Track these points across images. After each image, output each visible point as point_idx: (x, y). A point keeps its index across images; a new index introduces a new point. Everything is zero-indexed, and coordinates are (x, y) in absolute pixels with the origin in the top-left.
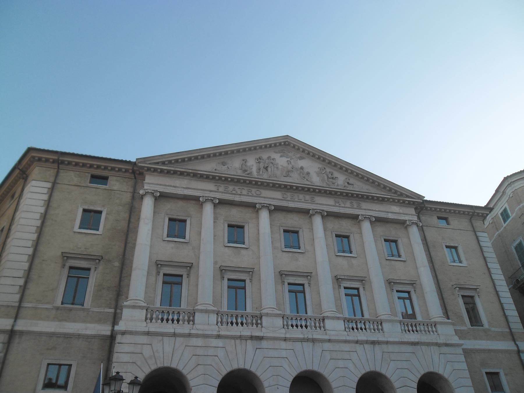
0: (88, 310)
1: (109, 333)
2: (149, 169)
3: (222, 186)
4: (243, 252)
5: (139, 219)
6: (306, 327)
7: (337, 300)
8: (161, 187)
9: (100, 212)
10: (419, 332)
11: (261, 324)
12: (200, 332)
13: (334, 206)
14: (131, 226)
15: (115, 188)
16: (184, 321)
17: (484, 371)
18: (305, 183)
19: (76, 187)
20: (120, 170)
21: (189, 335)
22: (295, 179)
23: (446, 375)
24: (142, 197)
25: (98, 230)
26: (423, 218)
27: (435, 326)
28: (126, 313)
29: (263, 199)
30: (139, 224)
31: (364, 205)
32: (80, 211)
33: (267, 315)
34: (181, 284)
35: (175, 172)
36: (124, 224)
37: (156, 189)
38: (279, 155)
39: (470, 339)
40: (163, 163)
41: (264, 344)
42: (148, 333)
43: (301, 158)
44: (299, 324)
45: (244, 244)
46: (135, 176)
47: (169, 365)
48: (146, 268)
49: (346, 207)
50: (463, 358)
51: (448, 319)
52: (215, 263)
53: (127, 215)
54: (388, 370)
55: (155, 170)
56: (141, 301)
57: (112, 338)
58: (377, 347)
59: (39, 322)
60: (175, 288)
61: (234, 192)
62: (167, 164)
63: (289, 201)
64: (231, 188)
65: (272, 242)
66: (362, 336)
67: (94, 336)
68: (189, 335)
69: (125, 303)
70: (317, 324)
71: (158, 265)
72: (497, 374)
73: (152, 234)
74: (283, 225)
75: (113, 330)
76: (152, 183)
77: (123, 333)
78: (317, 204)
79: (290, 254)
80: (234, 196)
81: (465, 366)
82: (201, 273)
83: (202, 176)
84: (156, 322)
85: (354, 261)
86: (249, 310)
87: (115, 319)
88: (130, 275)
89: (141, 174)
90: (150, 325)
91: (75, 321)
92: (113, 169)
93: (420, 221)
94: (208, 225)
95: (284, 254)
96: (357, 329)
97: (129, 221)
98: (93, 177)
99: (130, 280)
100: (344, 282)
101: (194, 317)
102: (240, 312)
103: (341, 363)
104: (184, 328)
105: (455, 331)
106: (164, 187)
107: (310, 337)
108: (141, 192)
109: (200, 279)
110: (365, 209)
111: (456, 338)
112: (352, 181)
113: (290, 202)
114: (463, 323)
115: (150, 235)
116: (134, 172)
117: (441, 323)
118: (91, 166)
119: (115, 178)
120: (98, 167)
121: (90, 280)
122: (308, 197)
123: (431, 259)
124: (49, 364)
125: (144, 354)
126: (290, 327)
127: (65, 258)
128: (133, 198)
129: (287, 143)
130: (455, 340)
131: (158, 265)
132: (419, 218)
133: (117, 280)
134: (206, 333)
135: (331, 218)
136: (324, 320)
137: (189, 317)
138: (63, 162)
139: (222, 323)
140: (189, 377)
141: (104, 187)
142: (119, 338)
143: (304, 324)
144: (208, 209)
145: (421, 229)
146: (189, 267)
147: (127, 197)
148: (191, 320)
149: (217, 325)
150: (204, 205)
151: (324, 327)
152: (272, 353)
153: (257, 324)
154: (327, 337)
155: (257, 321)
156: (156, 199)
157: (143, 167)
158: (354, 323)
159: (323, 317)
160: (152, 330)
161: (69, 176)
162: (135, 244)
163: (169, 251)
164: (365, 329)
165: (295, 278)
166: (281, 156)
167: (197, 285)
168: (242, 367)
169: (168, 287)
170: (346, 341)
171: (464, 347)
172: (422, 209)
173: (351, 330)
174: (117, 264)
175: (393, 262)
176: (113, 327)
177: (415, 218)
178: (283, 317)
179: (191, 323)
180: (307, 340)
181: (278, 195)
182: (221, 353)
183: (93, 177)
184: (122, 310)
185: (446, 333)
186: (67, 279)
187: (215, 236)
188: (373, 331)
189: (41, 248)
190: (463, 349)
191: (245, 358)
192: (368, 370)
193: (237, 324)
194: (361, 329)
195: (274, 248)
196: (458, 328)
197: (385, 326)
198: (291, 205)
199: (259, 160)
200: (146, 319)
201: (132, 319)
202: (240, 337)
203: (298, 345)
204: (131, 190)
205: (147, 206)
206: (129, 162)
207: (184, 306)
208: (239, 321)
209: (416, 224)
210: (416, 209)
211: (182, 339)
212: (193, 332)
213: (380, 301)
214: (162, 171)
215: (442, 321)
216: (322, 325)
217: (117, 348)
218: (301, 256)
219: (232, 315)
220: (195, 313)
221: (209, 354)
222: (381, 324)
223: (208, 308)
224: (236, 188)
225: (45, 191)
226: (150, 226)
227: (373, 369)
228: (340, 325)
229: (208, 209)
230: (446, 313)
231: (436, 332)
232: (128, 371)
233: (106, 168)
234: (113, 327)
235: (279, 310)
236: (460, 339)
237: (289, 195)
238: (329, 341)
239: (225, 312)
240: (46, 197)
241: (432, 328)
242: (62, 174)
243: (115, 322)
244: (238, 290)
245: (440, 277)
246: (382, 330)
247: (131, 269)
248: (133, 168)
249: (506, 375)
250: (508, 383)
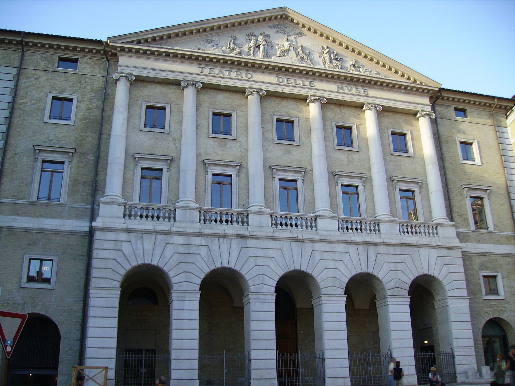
0: (64, 205)
1: (87, 229)
2: (123, 49)
3: (207, 67)
4: (230, 144)
5: (113, 106)
6: (296, 226)
7: (332, 198)
8: (137, 69)
9: (71, 100)
10: (418, 234)
11: (248, 223)
12: (181, 230)
13: (336, 92)
14: (106, 114)
15: (86, 72)
16: (164, 218)
17: (481, 274)
18: (305, 65)
19: (44, 72)
20: (91, 51)
21: (170, 233)
22: (291, 60)
23: (440, 278)
24: (116, 81)
25: (69, 120)
26: (438, 109)
27: (436, 228)
28: (103, 209)
29: (253, 83)
30: (113, 113)
31: (372, 92)
32: (50, 97)
33: (254, 213)
34: (161, 179)
35: (152, 53)
36: (97, 113)
37: (131, 72)
38: (275, 30)
39: (472, 243)
40: (139, 42)
41: (251, 243)
42: (127, 231)
43: (301, 34)
44: (289, 223)
45: (231, 135)
46: (107, 58)
47: (149, 262)
48: (122, 161)
49: (350, 94)
50: (460, 261)
51: (452, 220)
52: (198, 156)
53: (100, 103)
54: (383, 273)
55: (130, 50)
56: (119, 196)
57: (91, 232)
58: (372, 248)
59: (17, 217)
60: (155, 183)
61: (221, 75)
62: (142, 43)
63: (284, 85)
64: (216, 71)
65: (263, 133)
66: (358, 237)
67: (71, 232)
68: (170, 233)
69: (102, 199)
70: (309, 224)
71: (135, 158)
72: (495, 277)
73: (128, 123)
74: (276, 113)
75: (91, 227)
76: (127, 64)
77: (103, 229)
78: (317, 89)
79: (283, 147)
80: (220, 79)
81: (461, 269)
82: (182, 167)
83: (183, 56)
84: (135, 219)
85: (355, 156)
86: (235, 208)
87: (93, 216)
88: (106, 169)
89: (115, 55)
90: (128, 221)
91: (52, 217)
92: (83, 50)
93: (434, 113)
94: (188, 112)
95: (277, 146)
96: (352, 229)
97: (103, 110)
98: (61, 59)
99: (106, 175)
100: (342, 179)
101: (175, 214)
102: (225, 209)
103: (331, 264)
104: (164, 226)
105: (458, 234)
106: (140, 70)
107: (300, 236)
108: (115, 76)
109: (181, 174)
110: (372, 97)
111: (457, 240)
112: (362, 60)
113: (284, 87)
114: (468, 226)
115: (125, 126)
116: (106, 53)
117: (442, 225)
118: (59, 47)
119: (85, 60)
120: (67, 48)
121: (65, 174)
122: (307, 83)
123: (442, 156)
124: (30, 259)
125: (124, 250)
126: (279, 226)
127: (37, 151)
128: (106, 84)
129: (284, 16)
130: (456, 243)
131: (135, 158)
132: (433, 108)
133: (93, 174)
134: (188, 230)
135: (332, 107)
136: (316, 219)
137: (169, 214)
138: (27, 44)
139: (205, 220)
140: (171, 274)
141: (72, 71)
142: (98, 235)
143: (294, 223)
144: (190, 93)
145: (434, 123)
146: (171, 161)
147: (99, 82)
148: (171, 217)
149: (200, 222)
150: (185, 90)
151: (316, 227)
152: (260, 253)
153: (243, 223)
154: (317, 237)
155: (243, 220)
156: (131, 84)
157: (115, 48)
158: (347, 226)
159: (316, 216)
160: (131, 226)
161: (35, 59)
162: (109, 135)
163: (146, 141)
164: (361, 230)
165: (287, 174)
166: (277, 32)
167: (178, 180)
168: (225, 265)
169: (147, 183)
170: (338, 242)
171: (464, 250)
172: (437, 98)
173: (345, 230)
174: (91, 157)
175: (399, 158)
176: (91, 223)
177: (429, 109)
178: (271, 216)
179: (172, 220)
180: (296, 240)
181: (272, 79)
182: (203, 251)
183: (61, 59)
184: (99, 206)
185: (448, 234)
186: (41, 173)
187: (198, 126)
188: (368, 232)
189: (11, 140)
190: (462, 252)
191: (226, 256)
192: (359, 271)
193: (221, 222)
194: (356, 229)
195: (264, 138)
196: (461, 230)
197: (382, 226)
198: (287, 90)
199: (250, 37)
200: (125, 216)
201: (109, 215)
202: (224, 236)
203: (287, 244)
204: (104, 74)
205: (121, 91)
206: (100, 42)
207: (164, 202)
208: (224, 219)
209: (429, 115)
210: (431, 98)
211: (163, 236)
212: (174, 229)
213: (379, 199)
214: (138, 51)
215: (445, 223)
216: (314, 224)
217: (96, 245)
218: (295, 148)
219: (216, 212)
220: (175, 210)
221: (191, 252)
222: (378, 225)
223: (190, 205)
224: (223, 70)
225: (11, 77)
226: (125, 115)
227: (365, 270)
228: (333, 225)
229: (190, 93)
230: (450, 215)
231: (437, 234)
232: (108, 267)
233: (75, 49)
234: (91, 223)
235: (267, 208)
236: (461, 242)
237: (284, 79)
238: (321, 241)
239: (208, 209)
240: (12, 84)
241: (433, 230)
242: (28, 57)
243: (93, 217)
244: (224, 186)
245: (449, 176)
246: (379, 231)
247: (107, 163)
248: (104, 49)
249: (503, 278)
250: (504, 286)
